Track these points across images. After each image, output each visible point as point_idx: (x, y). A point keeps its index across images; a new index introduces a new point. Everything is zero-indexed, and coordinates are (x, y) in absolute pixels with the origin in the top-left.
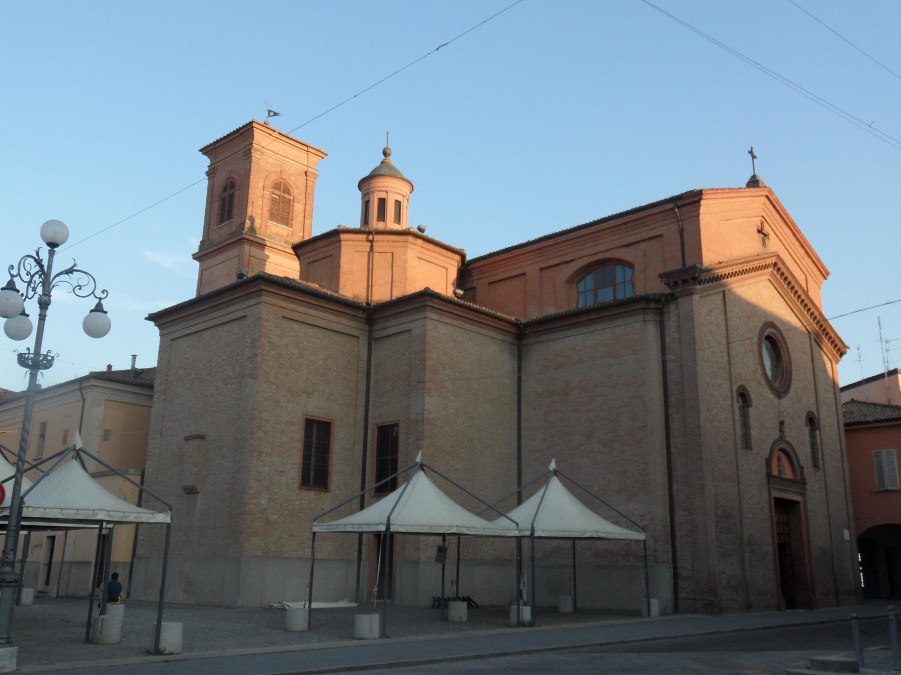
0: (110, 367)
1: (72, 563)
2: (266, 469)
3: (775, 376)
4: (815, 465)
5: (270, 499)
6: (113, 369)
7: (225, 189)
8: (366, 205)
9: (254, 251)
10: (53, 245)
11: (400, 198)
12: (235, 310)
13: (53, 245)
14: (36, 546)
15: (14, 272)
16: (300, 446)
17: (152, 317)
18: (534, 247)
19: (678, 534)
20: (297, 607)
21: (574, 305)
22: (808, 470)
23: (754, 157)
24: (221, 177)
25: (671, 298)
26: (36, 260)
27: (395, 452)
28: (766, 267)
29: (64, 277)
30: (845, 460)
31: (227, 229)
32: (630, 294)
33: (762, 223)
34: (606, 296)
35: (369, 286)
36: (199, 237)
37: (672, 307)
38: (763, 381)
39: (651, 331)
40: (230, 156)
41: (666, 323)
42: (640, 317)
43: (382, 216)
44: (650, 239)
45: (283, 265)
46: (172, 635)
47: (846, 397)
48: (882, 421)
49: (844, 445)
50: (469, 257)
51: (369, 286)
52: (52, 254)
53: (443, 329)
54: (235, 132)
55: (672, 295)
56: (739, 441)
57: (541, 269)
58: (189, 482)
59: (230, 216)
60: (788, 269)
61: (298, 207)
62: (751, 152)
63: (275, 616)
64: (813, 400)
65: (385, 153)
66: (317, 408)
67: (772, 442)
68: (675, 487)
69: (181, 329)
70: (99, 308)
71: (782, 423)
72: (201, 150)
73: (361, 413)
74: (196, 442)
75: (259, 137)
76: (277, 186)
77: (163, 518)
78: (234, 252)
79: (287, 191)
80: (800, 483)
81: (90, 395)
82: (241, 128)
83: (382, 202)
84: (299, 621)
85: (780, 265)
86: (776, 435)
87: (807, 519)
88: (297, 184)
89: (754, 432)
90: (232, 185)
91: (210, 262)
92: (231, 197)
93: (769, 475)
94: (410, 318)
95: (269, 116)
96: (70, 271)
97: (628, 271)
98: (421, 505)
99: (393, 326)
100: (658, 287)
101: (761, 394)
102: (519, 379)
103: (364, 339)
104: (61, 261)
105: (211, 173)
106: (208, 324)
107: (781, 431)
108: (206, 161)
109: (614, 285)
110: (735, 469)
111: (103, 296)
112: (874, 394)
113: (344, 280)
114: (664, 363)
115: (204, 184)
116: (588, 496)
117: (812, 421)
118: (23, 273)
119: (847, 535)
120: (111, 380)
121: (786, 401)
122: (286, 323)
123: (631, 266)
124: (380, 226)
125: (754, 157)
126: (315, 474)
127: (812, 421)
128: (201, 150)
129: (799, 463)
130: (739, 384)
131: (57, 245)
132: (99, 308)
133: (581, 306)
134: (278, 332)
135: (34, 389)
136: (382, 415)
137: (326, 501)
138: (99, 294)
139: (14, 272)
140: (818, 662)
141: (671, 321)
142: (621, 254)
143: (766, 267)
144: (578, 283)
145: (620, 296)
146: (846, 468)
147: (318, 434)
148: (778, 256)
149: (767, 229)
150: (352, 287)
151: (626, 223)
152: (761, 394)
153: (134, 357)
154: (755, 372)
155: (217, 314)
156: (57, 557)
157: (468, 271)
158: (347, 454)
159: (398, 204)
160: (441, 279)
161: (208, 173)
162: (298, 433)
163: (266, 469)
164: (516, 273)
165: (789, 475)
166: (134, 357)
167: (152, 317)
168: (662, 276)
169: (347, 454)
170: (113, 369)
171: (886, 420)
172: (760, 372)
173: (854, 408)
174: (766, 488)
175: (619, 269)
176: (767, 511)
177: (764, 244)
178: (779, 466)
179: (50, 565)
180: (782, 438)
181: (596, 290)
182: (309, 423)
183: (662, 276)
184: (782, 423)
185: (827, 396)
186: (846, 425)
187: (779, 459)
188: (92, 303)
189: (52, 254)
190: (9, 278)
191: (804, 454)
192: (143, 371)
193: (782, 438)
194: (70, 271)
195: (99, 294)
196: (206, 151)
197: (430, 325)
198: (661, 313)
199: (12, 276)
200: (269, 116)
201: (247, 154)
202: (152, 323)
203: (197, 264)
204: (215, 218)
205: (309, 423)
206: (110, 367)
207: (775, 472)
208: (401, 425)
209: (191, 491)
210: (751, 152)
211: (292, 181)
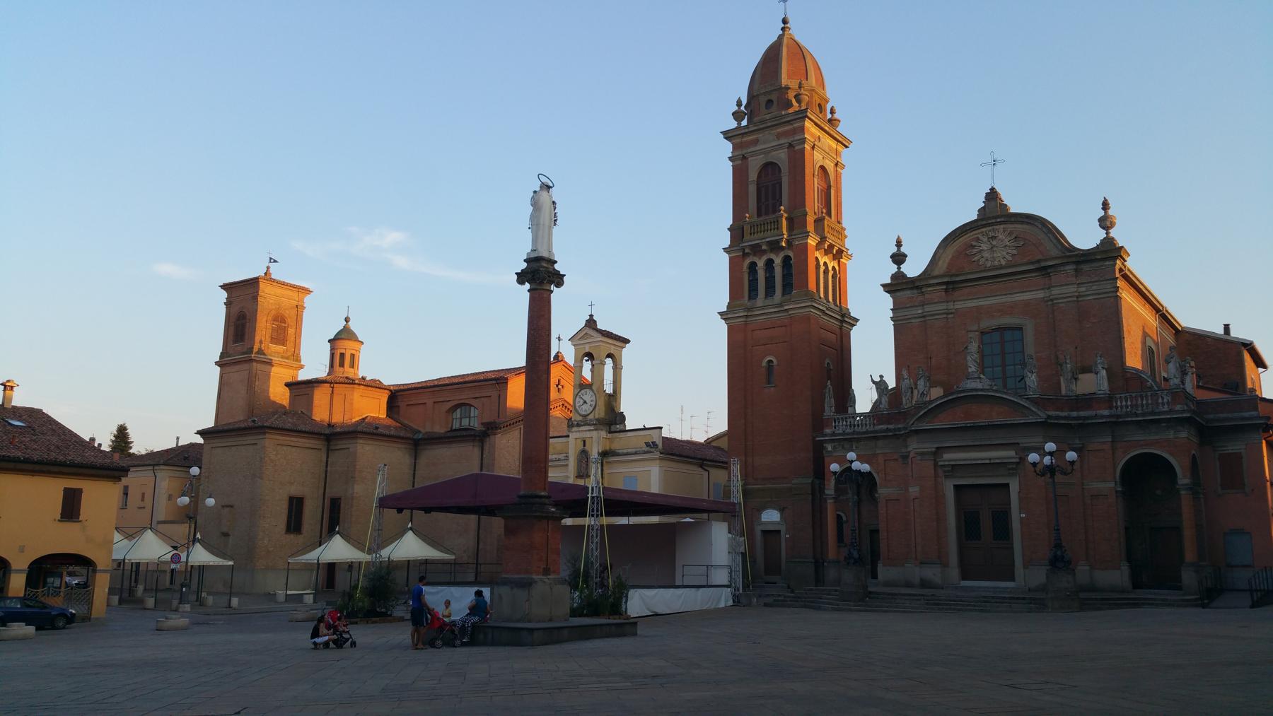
8: (332, 356)
9: (260, 367)
12: (250, 439)
20: (281, 593)
24: (235, 309)
31: (239, 347)
35: (331, 414)
39: (477, 451)
40: (243, 299)
43: (342, 365)
45: (278, 393)
46: (235, 601)
51: (331, 414)
53: (367, 448)
58: (225, 530)
61: (291, 331)
63: (271, 597)
65: (347, 320)
66: (295, 490)
73: (321, 491)
74: (227, 510)
75: (262, 285)
76: (276, 319)
77: (231, 563)
78: (246, 366)
79: (283, 321)
83: (342, 355)
84: (281, 598)
88: (290, 314)
91: (228, 369)
92: (243, 326)
98: (338, 550)
103: (324, 450)
105: (228, 304)
108: (224, 294)
113: (315, 410)
116: (427, 537)
126: (294, 524)
136: (333, 492)
137: (300, 539)
141: (486, 447)
142: (472, 402)
147: (296, 505)
150: (320, 413)
157: (397, 397)
158: (312, 515)
159: (353, 356)
160: (374, 408)
162: (285, 506)
169: (312, 515)
182: (291, 499)
197: (359, 447)
198: (482, 442)
201: (255, 298)
203: (218, 369)
204: (231, 338)
205: (291, 499)
209: (226, 535)
211: (286, 314)
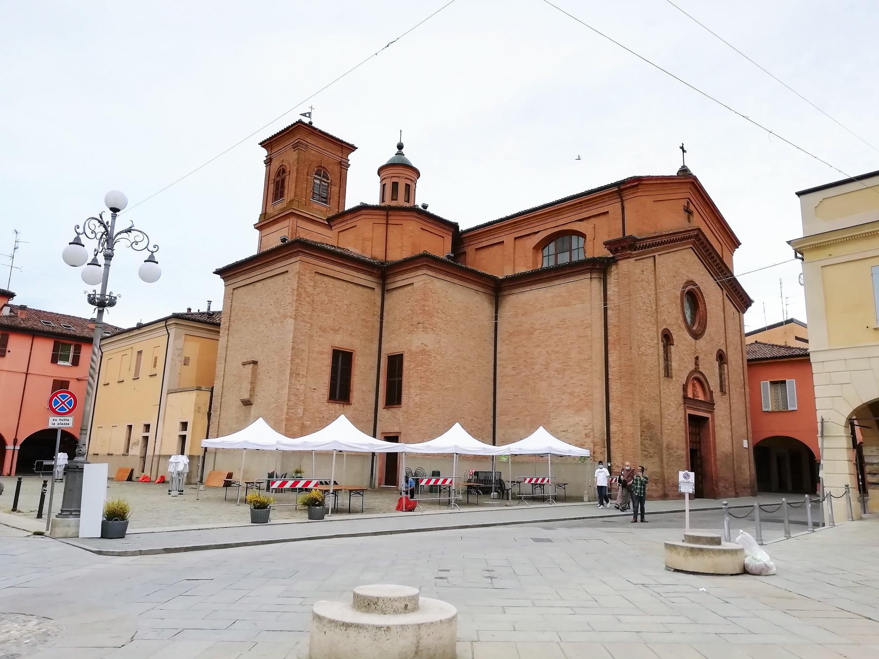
0: (189, 310)
1: (160, 456)
2: (302, 387)
3: (693, 323)
4: (722, 391)
5: (304, 409)
6: (192, 311)
7: (278, 175)
10: (115, 210)
11: (409, 182)
13: (115, 210)
14: (135, 444)
15: (80, 230)
16: (328, 370)
17: (218, 272)
18: (511, 221)
19: (612, 440)
21: (540, 266)
22: (717, 394)
23: (684, 151)
24: (275, 165)
25: (613, 261)
26: (99, 222)
27: (401, 375)
28: (690, 237)
29: (124, 235)
30: (747, 387)
32: (582, 257)
33: (688, 203)
34: (564, 258)
36: (259, 211)
37: (614, 268)
38: (683, 326)
41: (608, 280)
42: (588, 276)
44: (598, 215)
47: (749, 340)
48: (777, 358)
49: (746, 376)
50: (462, 227)
52: (114, 217)
54: (285, 130)
55: (613, 258)
56: (662, 372)
57: (516, 239)
59: (282, 196)
60: (707, 240)
62: (682, 148)
64: (723, 341)
66: (342, 342)
67: (688, 372)
68: (611, 405)
69: (240, 281)
70: (151, 260)
71: (697, 358)
72: (260, 144)
80: (710, 405)
81: (172, 331)
82: (290, 127)
85: (701, 236)
86: (692, 367)
87: (714, 431)
89: (674, 365)
90: (284, 171)
92: (283, 180)
93: (685, 397)
94: (412, 274)
95: (309, 113)
96: (129, 231)
97: (581, 239)
99: (400, 280)
100: (604, 252)
101: (681, 336)
102: (496, 324)
103: (378, 290)
104: (121, 224)
105: (268, 162)
106: (260, 277)
107: (696, 364)
108: (264, 153)
109: (570, 250)
110: (658, 393)
111: (155, 250)
112: (777, 338)
114: (606, 310)
115: (263, 168)
117: (721, 357)
118: (88, 232)
119: (745, 444)
120: (188, 319)
121: (701, 342)
122: (318, 277)
123: (583, 236)
124: (394, 204)
125: (684, 151)
127: (721, 357)
128: (260, 144)
129: (709, 388)
130: (664, 327)
131: (118, 210)
132: (151, 260)
133: (545, 265)
134: (312, 284)
135: (96, 322)
138: (151, 248)
139: (80, 230)
140: (689, 536)
142: (577, 227)
143: (690, 237)
144: (543, 249)
145: (575, 259)
146: (747, 394)
147: (342, 361)
148: (699, 229)
149: (692, 208)
151: (580, 203)
152: (681, 336)
153: (210, 302)
154: (677, 319)
155: (267, 269)
156: (150, 452)
161: (266, 162)
162: (328, 361)
163: (302, 387)
164: (496, 241)
165: (701, 397)
166: (210, 302)
167: (218, 272)
168: (606, 244)
170: (192, 311)
171: (780, 357)
172: (681, 318)
173: (755, 348)
174: (682, 407)
175: (574, 238)
176: (683, 424)
177: (689, 220)
178: (694, 390)
179: (144, 458)
180: (696, 370)
181: (556, 255)
183: (606, 244)
184: (697, 358)
185: (734, 338)
186: (748, 360)
187: (694, 386)
188: (146, 255)
189: (114, 217)
190: (76, 235)
191: (714, 383)
192: (214, 313)
193: (696, 370)
194: (129, 231)
195: (151, 248)
196: (266, 144)
199: (78, 234)
200: (309, 113)
202: (219, 276)
203: (257, 232)
204: (270, 197)
206: (189, 310)
207: (690, 395)
208: (405, 355)
210: (682, 148)
